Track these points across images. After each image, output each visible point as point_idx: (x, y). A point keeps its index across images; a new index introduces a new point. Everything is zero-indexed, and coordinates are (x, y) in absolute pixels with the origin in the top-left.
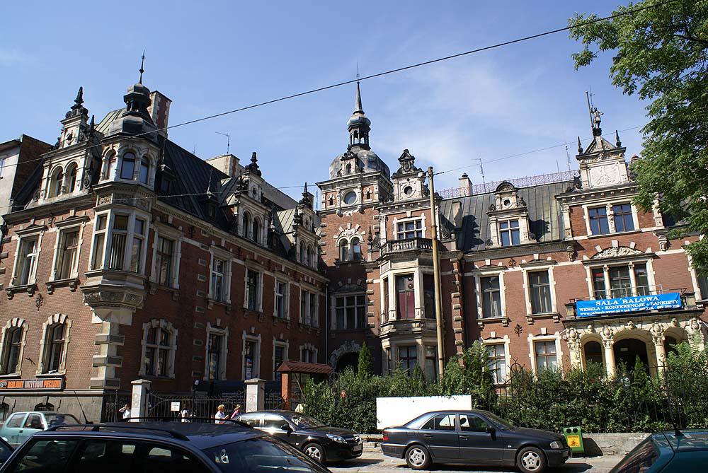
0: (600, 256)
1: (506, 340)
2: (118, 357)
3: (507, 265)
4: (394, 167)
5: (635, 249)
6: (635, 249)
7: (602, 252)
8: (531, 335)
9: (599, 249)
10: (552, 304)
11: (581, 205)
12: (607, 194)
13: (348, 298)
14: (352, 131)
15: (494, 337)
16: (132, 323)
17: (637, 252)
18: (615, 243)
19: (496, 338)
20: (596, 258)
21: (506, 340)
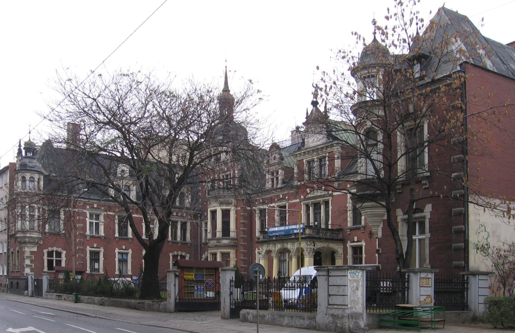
0: (309, 196)
7: (310, 193)
19: (358, 241)
21: (363, 243)
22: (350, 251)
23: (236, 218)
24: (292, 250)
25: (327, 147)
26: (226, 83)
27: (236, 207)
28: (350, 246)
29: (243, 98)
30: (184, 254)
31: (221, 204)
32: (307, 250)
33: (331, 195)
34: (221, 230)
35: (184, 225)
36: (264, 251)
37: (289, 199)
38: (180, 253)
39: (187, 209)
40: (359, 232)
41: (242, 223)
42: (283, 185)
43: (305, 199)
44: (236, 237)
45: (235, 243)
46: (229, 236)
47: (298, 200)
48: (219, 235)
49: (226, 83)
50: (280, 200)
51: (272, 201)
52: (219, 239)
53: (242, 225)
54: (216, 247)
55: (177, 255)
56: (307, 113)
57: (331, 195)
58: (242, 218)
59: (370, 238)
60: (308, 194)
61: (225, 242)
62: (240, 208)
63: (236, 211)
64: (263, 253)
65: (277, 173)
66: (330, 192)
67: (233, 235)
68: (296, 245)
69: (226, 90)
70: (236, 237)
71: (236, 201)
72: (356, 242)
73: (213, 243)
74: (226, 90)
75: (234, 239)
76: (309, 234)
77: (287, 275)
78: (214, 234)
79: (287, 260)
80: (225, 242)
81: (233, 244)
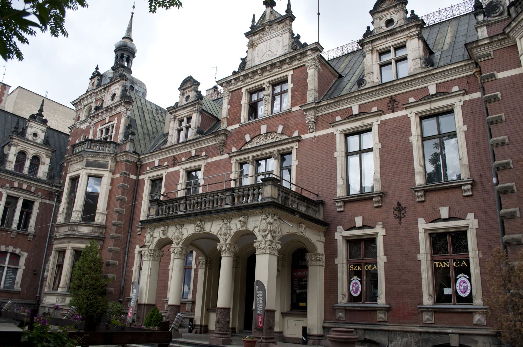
0: (249, 146)
1: (380, 231)
2: (490, 146)
3: (385, 109)
4: (10, 144)
5: (282, 134)
6: (282, 134)
7: (250, 142)
8: (340, 228)
9: (248, 138)
10: (14, 221)
11: (241, 88)
12: (264, 69)
13: (25, 201)
14: (119, 53)
15: (447, 217)
16: (456, 86)
17: (285, 137)
18: (263, 129)
19: (364, 227)
20: (246, 147)
21: (380, 231)
22: (342, 249)
23: (111, 191)
24: (221, 238)
25: (293, 59)
26: (129, 30)
27: (114, 174)
28: (344, 237)
29: (119, 200)
30: (18, 251)
31: (89, 165)
32: (265, 237)
33: (298, 140)
34: (81, 210)
35: (28, 205)
36: (156, 240)
37: (207, 157)
38: (11, 249)
39: (39, 181)
40: (368, 206)
41: (119, 199)
42: (199, 136)
43: (240, 152)
44: (104, 223)
45: (101, 233)
46: (94, 220)
47: (226, 156)
48: (76, 216)
49: (129, 30)
50: (191, 159)
51: (175, 162)
52: (74, 224)
53: (119, 202)
54: (68, 237)
55: (6, 253)
56: (253, 21)
57: (298, 140)
58: (120, 190)
59: (400, 218)
60: (247, 143)
61: (85, 230)
62: (118, 175)
63: (113, 180)
64: (152, 247)
65: (189, 119)
66: (296, 134)
67: (99, 219)
68: (235, 225)
69: (128, 37)
70: (104, 223)
71: (114, 165)
72: (359, 228)
73: (65, 230)
74: (128, 37)
75: (101, 226)
76: (272, 197)
77: (190, 297)
78: (69, 215)
79: (194, 267)
80: (85, 230)
81: (96, 234)
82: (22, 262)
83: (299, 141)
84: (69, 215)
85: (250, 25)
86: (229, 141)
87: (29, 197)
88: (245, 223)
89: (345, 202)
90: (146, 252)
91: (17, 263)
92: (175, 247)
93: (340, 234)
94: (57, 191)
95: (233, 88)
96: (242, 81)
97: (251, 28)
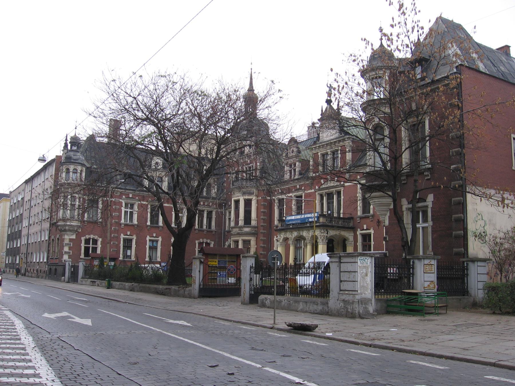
0: (323, 186)
21: (372, 231)
25: (340, 141)
33: (343, 186)
36: (282, 238)
37: (305, 190)
38: (205, 240)
43: (320, 189)
44: (256, 225)
47: (313, 191)
48: (241, 223)
50: (297, 190)
51: (289, 191)
52: (241, 227)
54: (239, 234)
56: (322, 110)
57: (343, 186)
60: (322, 184)
61: (247, 230)
63: (257, 200)
64: (281, 241)
65: (295, 165)
66: (342, 183)
67: (254, 223)
70: (256, 225)
71: (257, 191)
73: (236, 230)
74: (251, 89)
75: (254, 227)
77: (302, 262)
78: (237, 222)
79: (303, 247)
80: (247, 230)
81: (253, 232)
82: (99, 243)
83: (344, 186)
84: (237, 222)
85: (320, 113)
86: (315, 183)
87: (210, 209)
88: (314, 232)
89: (361, 218)
90: (279, 243)
91: (96, 244)
92: (290, 242)
93: (359, 232)
94: (224, 203)
95: (314, 152)
96: (318, 149)
97: (321, 115)
